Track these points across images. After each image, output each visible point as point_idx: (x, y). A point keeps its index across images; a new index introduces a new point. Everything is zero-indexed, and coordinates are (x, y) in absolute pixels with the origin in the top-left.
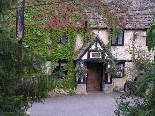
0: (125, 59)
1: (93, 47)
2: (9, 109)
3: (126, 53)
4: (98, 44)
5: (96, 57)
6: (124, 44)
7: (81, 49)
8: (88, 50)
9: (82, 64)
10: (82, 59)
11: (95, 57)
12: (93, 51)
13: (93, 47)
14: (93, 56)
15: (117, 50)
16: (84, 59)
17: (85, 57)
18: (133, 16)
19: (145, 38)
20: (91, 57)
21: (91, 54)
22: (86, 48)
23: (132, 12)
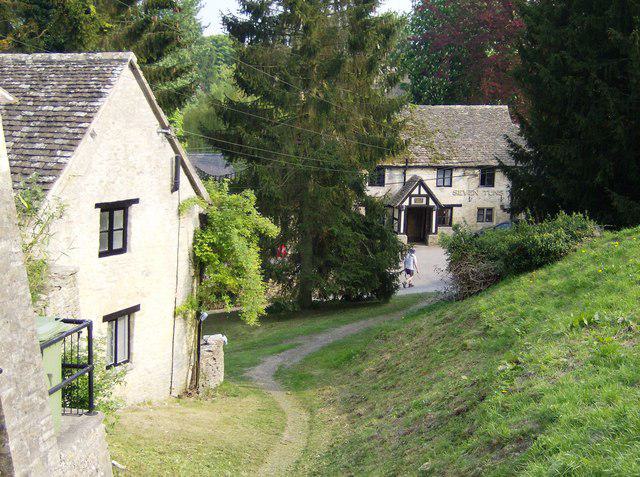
1: (416, 192)
4: (422, 188)
12: (415, 196)
17: (406, 203)
20: (413, 203)
21: (413, 199)
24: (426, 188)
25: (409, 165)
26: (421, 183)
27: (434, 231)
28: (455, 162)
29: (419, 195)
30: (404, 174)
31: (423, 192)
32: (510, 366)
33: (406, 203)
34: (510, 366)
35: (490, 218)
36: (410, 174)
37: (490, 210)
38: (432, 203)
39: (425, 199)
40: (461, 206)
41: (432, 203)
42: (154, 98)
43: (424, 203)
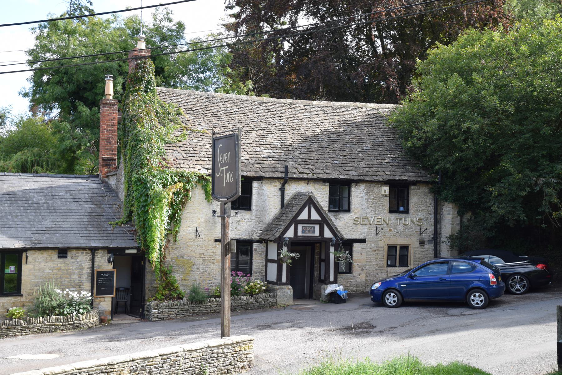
0: (354, 237)
1: (304, 216)
2: (40, 28)
3: (355, 225)
4: (313, 211)
5: (308, 233)
6: (352, 210)
7: (278, 218)
8: (295, 221)
9: (332, 246)
10: (285, 238)
11: (306, 233)
12: (303, 222)
13: (304, 216)
14: (303, 233)
15: (205, 234)
16: (289, 238)
17: (290, 234)
18: (361, 157)
19: (388, 198)
20: (300, 233)
21: (300, 227)
22: (290, 216)
23: (359, 150)
24: (319, 211)
25: (290, 176)
26: (311, 202)
27: (332, 279)
28: (354, 175)
29: (309, 221)
30: (282, 190)
31: (315, 216)
32: (524, 12)
33: (290, 234)
34: (524, 12)
35: (404, 261)
36: (292, 189)
37: (405, 248)
38: (328, 234)
39: (317, 227)
40: (363, 241)
41: (328, 234)
42: (62, 175)
43: (317, 233)
